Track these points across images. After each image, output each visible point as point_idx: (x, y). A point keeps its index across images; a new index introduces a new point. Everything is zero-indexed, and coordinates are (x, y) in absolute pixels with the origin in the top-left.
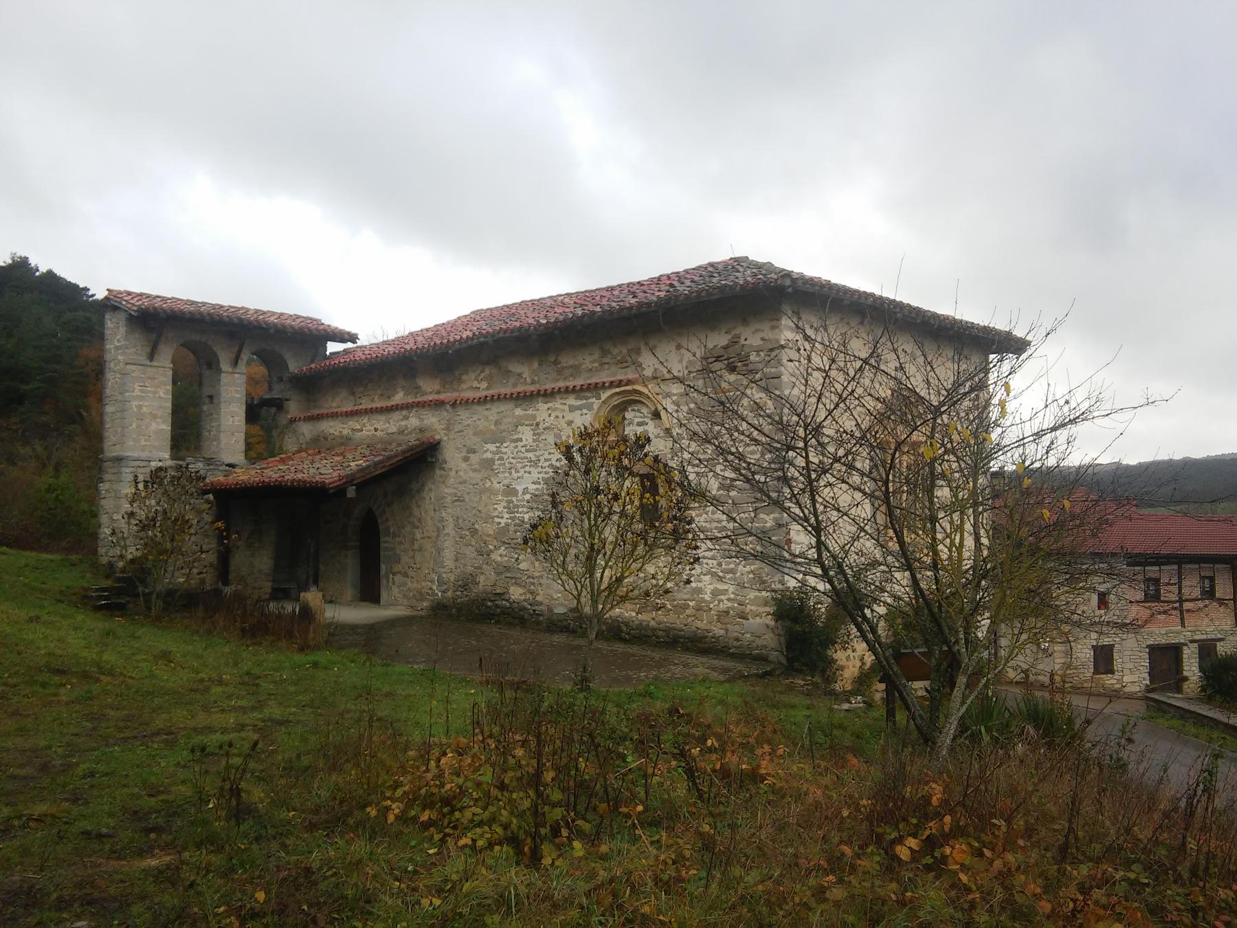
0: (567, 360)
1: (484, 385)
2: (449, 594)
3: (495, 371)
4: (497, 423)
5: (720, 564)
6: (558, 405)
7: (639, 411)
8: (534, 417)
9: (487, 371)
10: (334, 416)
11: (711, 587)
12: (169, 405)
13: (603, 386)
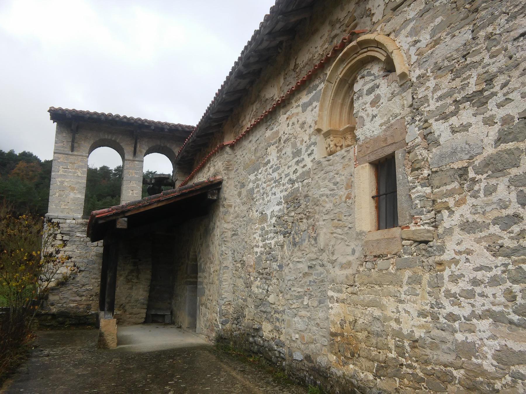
2: (228, 326)
5: (511, 297)
6: (294, 111)
7: (369, 74)
11: (495, 344)
12: (85, 181)
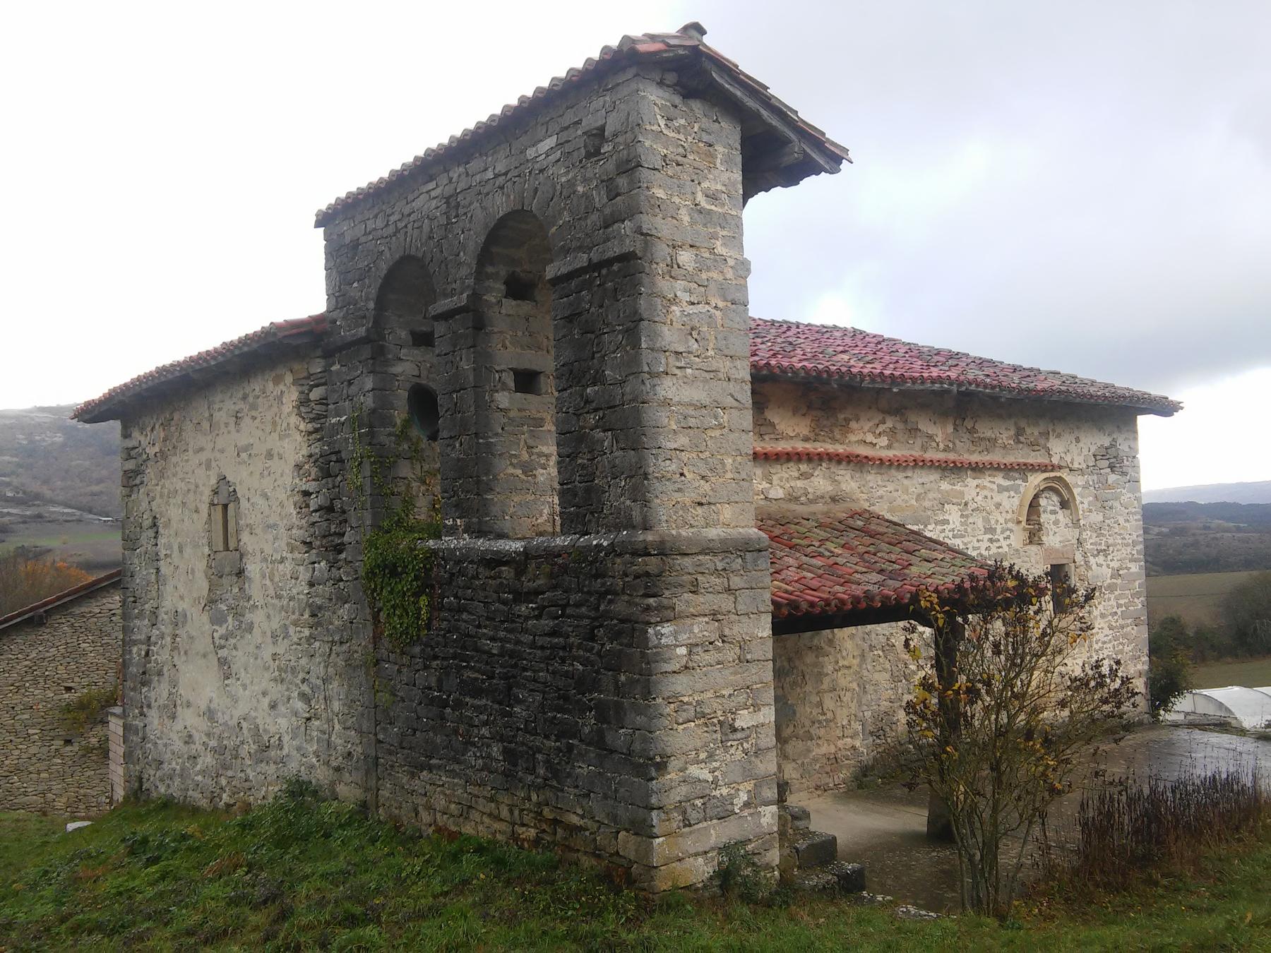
0: (986, 430)
1: (884, 441)
3: (900, 426)
4: (919, 497)
8: (962, 493)
9: (889, 424)
10: (857, 462)
13: (1033, 468)
